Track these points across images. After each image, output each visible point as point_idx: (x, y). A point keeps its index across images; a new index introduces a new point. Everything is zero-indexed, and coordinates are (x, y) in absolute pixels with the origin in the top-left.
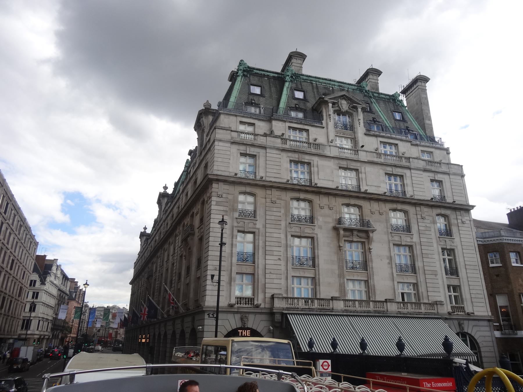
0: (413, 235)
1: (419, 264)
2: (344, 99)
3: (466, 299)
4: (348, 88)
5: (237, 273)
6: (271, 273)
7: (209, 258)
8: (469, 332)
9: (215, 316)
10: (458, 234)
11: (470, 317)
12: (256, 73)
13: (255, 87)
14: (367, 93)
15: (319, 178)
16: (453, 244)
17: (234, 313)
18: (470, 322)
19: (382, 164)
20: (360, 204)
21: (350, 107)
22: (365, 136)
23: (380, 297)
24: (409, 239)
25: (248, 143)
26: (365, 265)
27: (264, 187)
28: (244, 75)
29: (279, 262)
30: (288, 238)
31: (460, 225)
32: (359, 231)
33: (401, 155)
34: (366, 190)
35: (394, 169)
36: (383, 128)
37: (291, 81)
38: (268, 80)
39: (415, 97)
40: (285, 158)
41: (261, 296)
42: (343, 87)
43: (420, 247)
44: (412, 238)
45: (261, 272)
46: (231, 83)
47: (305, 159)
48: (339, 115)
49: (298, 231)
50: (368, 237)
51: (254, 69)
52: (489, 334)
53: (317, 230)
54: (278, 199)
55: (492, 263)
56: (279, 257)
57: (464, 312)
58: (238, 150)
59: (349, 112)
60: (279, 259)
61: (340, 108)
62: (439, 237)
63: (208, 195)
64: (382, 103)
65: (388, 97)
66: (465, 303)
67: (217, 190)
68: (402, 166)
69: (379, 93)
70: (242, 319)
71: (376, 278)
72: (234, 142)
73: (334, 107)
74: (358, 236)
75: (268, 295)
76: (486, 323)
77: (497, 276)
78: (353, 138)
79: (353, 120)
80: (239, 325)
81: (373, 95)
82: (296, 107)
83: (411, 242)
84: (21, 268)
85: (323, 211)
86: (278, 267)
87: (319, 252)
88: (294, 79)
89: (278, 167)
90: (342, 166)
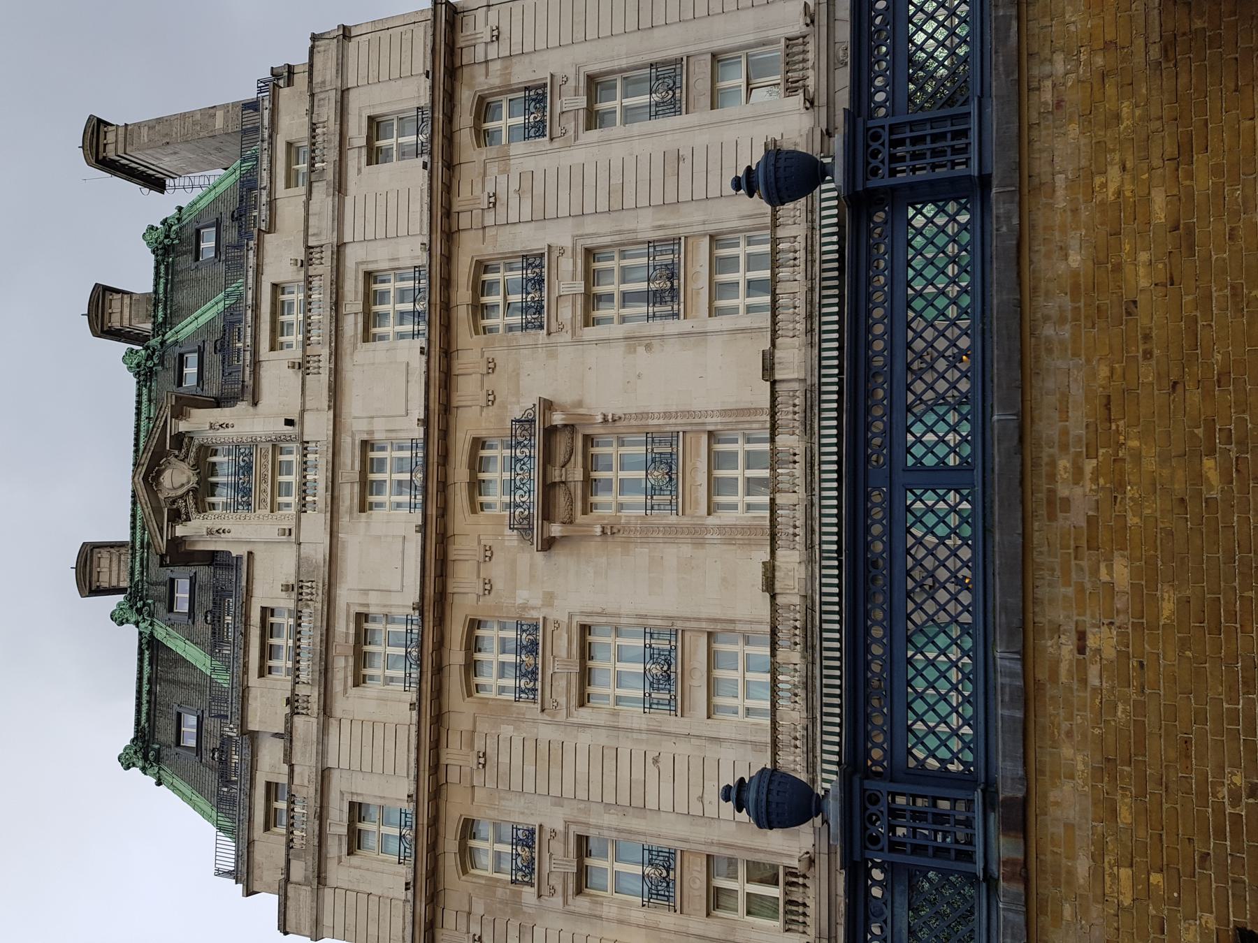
0: (549, 246)
6: (701, 798)
10: (536, 58)
12: (148, 720)
14: (153, 353)
16: (572, 83)
19: (336, 354)
20: (467, 447)
21: (182, 456)
22: (260, 406)
24: (566, 264)
25: (317, 832)
27: (437, 794)
29: (666, 763)
30: (589, 722)
32: (548, 458)
40: (348, 702)
43: (588, 220)
44: (562, 251)
47: (347, 634)
48: (212, 489)
56: (650, 760)
58: (340, 861)
59: (197, 458)
60: (656, 761)
62: (552, 139)
66: (772, 34)
68: (334, 277)
71: (697, 405)
72: (319, 877)
73: (187, 514)
78: (274, 446)
85: (498, 585)
90: (356, 501)
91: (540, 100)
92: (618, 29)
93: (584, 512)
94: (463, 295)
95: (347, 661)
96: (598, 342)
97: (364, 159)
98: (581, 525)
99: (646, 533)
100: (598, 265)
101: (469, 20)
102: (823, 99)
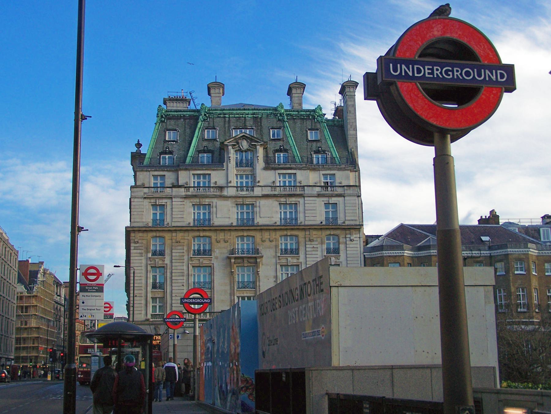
2: (244, 138)
6: (176, 296)
15: (218, 217)
19: (275, 196)
24: (295, 261)
35: (287, 199)
38: (184, 121)
44: (298, 259)
49: (198, 263)
56: (183, 284)
60: (183, 285)
67: (134, 238)
70: (155, 329)
84: (6, 284)
85: (219, 244)
87: (215, 277)
88: (207, 117)
89: (182, 213)
90: (238, 203)
93: (237, 266)
97: (326, 202)
98: (234, 266)
99: (232, 282)
101: (357, 232)
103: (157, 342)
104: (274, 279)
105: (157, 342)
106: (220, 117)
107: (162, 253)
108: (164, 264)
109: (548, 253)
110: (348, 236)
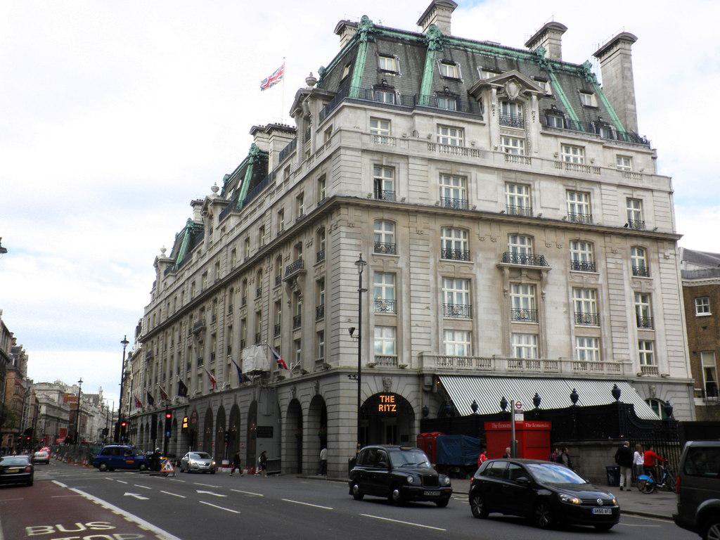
1: (604, 313)
2: (513, 81)
3: (661, 357)
4: (518, 58)
5: (376, 326)
7: (342, 307)
8: (662, 399)
9: (357, 378)
11: (666, 382)
12: (385, 36)
13: (386, 59)
17: (374, 375)
18: (664, 386)
20: (531, 234)
23: (552, 356)
26: (536, 315)
28: (370, 41)
29: (427, 312)
31: (661, 261)
33: (589, 163)
34: (541, 215)
36: (568, 125)
37: (437, 49)
39: (614, 66)
41: (406, 355)
42: (511, 56)
44: (597, 280)
45: (405, 324)
46: (671, 516)
50: (541, 279)
51: (382, 28)
52: (686, 401)
53: (476, 270)
54: (424, 228)
55: (700, 311)
56: (428, 305)
57: (658, 373)
60: (428, 308)
61: (507, 94)
63: (333, 222)
64: (565, 79)
65: (574, 69)
66: (660, 361)
69: (561, 63)
70: (384, 382)
74: (527, 276)
75: (415, 354)
76: (684, 388)
77: (705, 328)
79: (524, 112)
80: (381, 389)
81: (553, 67)
82: (445, 92)
83: (394, 268)
86: (427, 318)
89: (424, 184)
91: (644, 274)
92: (665, 306)
94: (583, 237)
95: (449, 170)
96: (568, 292)
100: (460, 181)
101: (672, 246)
102: (640, 380)
103: (387, 407)
104: (565, 309)
105: (387, 407)
106: (459, 49)
107: (391, 249)
108: (397, 268)
109: (709, 281)
110: (662, 251)
